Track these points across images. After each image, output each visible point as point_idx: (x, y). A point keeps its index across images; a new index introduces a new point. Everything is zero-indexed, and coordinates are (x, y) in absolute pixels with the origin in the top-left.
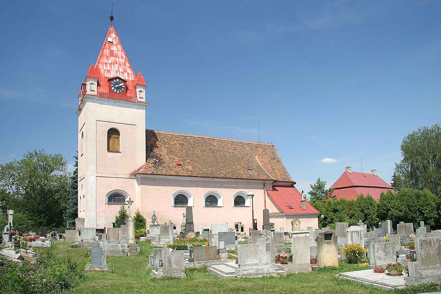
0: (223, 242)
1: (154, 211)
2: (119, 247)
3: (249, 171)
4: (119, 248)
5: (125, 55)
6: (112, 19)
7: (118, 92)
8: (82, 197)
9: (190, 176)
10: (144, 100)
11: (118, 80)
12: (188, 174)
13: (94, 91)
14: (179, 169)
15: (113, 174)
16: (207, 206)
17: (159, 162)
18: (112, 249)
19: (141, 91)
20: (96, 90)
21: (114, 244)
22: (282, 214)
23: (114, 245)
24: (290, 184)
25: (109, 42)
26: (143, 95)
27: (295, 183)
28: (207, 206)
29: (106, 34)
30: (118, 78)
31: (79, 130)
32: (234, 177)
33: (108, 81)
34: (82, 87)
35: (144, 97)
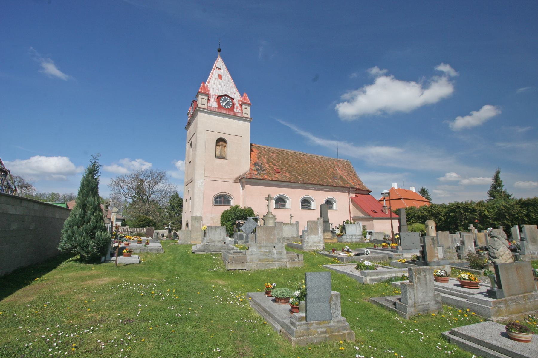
0: (441, 247)
1: (258, 212)
2: (274, 254)
3: (335, 180)
4: (273, 256)
5: (102, 285)
6: (219, 51)
7: (226, 107)
8: (188, 199)
9: (289, 182)
10: (249, 116)
11: (226, 97)
12: (287, 180)
13: (204, 105)
14: (278, 175)
15: (220, 178)
16: (302, 209)
17: (261, 169)
18: (264, 257)
19: (246, 108)
20: (206, 104)
21: (265, 249)
22: (368, 217)
23: (266, 252)
24: (367, 192)
25: (217, 68)
26: (248, 111)
27: (370, 192)
28: (302, 209)
29: (215, 60)
30: (226, 95)
31: (187, 141)
32: (325, 184)
33: (217, 98)
34: (192, 104)
35: (249, 114)
